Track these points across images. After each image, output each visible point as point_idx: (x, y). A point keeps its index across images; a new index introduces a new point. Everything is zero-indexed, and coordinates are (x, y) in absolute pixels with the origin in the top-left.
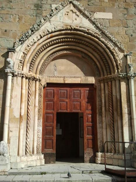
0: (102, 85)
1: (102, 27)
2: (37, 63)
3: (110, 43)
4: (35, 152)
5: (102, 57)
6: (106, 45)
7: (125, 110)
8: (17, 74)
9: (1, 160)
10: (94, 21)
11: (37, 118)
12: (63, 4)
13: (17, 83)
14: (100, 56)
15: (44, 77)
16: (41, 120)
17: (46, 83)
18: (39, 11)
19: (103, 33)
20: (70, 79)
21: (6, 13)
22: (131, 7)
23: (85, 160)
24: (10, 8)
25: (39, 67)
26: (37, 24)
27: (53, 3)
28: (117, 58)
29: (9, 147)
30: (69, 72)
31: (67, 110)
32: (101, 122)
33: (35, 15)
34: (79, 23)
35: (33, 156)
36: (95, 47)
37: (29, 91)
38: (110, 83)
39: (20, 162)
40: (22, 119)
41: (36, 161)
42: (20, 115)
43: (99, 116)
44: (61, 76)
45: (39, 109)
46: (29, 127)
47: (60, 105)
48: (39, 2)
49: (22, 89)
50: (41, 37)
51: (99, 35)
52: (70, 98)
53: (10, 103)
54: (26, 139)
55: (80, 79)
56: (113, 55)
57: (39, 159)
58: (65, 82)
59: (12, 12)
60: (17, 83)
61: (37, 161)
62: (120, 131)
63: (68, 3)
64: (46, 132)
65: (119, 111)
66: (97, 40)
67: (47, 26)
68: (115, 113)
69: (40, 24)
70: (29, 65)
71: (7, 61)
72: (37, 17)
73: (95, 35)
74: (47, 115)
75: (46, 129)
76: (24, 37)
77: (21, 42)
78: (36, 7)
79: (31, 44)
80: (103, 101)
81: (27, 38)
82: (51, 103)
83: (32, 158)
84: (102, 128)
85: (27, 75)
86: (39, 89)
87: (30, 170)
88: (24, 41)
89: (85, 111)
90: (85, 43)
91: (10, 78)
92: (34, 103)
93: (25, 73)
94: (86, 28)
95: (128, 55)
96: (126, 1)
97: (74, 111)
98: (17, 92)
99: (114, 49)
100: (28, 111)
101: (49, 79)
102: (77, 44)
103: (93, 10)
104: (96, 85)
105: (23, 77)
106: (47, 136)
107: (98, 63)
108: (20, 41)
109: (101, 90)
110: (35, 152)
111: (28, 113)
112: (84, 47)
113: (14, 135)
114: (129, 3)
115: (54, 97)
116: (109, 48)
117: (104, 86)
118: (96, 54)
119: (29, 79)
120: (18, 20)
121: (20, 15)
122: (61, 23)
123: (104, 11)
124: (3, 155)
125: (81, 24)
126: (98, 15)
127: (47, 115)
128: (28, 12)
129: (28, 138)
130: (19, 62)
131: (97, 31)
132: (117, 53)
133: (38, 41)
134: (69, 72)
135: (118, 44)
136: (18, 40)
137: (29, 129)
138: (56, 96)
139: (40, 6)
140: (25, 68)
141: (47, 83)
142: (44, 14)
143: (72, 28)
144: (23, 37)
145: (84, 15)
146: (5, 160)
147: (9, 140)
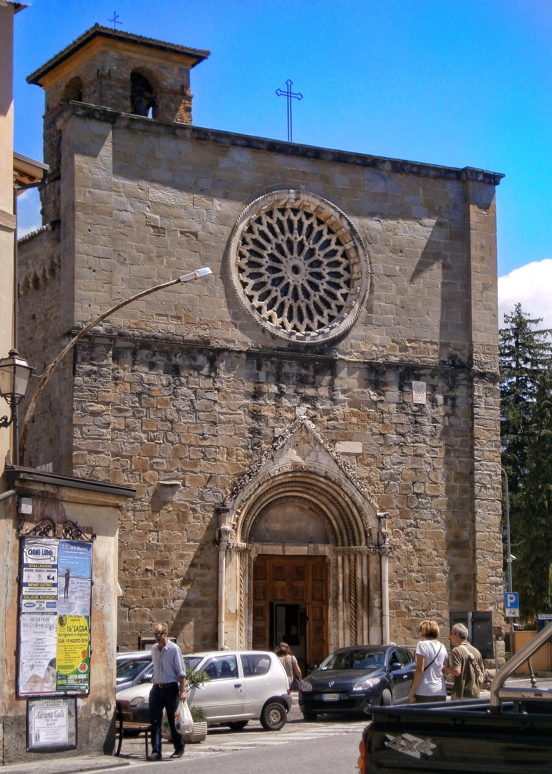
0: (340, 558)
5: (342, 511)
7: (490, 469)
14: (340, 512)
27: (277, 425)
32: (337, 618)
33: (250, 447)
36: (333, 497)
38: (352, 558)
43: (222, 649)
58: (284, 552)
62: (365, 632)
68: (360, 605)
80: (341, 585)
84: (337, 627)
102: (306, 490)
104: (330, 558)
107: (334, 522)
109: (337, 567)
112: (316, 494)
116: (354, 503)
118: (333, 508)
126: (342, 447)
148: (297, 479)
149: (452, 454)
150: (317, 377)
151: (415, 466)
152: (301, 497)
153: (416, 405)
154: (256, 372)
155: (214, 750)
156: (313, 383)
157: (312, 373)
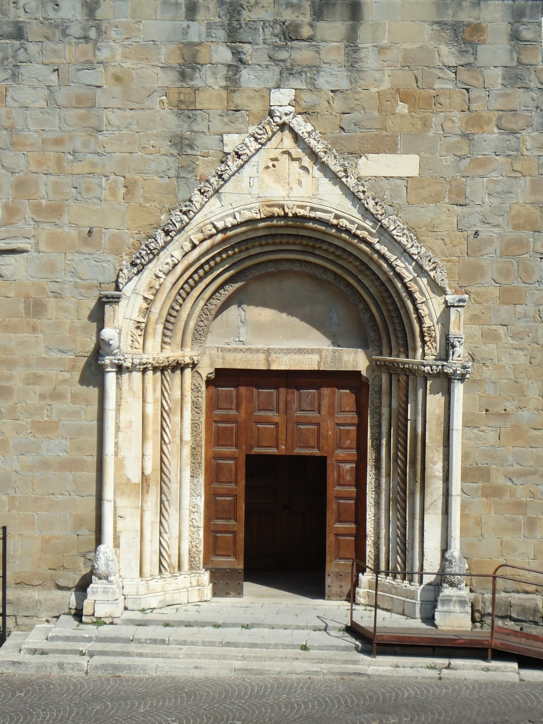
1: (380, 212)
2: (184, 315)
3: (402, 262)
4: (186, 566)
6: (393, 268)
8: (129, 365)
9: (103, 592)
10: (355, 191)
11: (187, 473)
12: (259, 137)
13: (131, 388)
15: (207, 353)
16: (202, 479)
17: (212, 370)
19: (383, 230)
20: (287, 358)
21: (88, 171)
22: (485, 128)
23: (326, 591)
24: (98, 154)
25: (192, 324)
26: (181, 211)
27: (228, 128)
28: (424, 310)
29: (118, 557)
30: (283, 339)
31: (277, 447)
33: (172, 173)
34: (311, 195)
35: (181, 578)
37: (163, 551)
39: (146, 594)
40: (148, 486)
41: (188, 591)
42: (143, 473)
44: (260, 346)
45: (194, 448)
46: (166, 503)
47: (256, 432)
48: (186, 126)
49: (144, 401)
50: (194, 246)
51: (371, 234)
52: (286, 413)
53: (116, 444)
54: (160, 533)
55: (316, 357)
56: (414, 301)
57: (196, 584)
59: (104, 166)
60: (131, 388)
61: (192, 588)
62: (417, 523)
63: (276, 128)
64: (214, 509)
65: (419, 467)
66: (367, 249)
67: (211, 212)
69: (188, 208)
70: (160, 327)
71: (103, 340)
72: (179, 180)
74: (219, 462)
75: (216, 502)
76: (144, 253)
77: (135, 270)
78: (175, 144)
79: (166, 268)
81: (151, 256)
82: (229, 427)
83: (177, 583)
85: (157, 363)
86: (193, 387)
87: (170, 614)
88: (143, 266)
89: (333, 452)
91: (111, 378)
92: (178, 433)
93: (151, 361)
94: (331, 212)
95: (454, 306)
96: (472, 109)
97: (299, 451)
99: (414, 280)
100: (160, 560)
103: (355, 147)
105: (144, 371)
106: (219, 522)
108: (133, 264)
109: (379, 392)
110: (186, 566)
111: (163, 466)
113: (129, 526)
114: (481, 116)
115: (238, 408)
116: (401, 278)
117: (388, 383)
119: (163, 370)
120: (125, 194)
121: (127, 175)
122: (254, 200)
123: (393, 150)
124: (108, 579)
125: (314, 201)
127: (219, 462)
128: (153, 166)
129: (166, 533)
130: (132, 325)
131: (368, 224)
132: (422, 294)
133: (184, 256)
134: (283, 339)
135: (427, 268)
136: (126, 263)
137: (168, 508)
138: (243, 406)
139: (187, 142)
140: (150, 343)
141: (217, 370)
142: (201, 171)
143: (286, 214)
144: (140, 253)
145: (324, 168)
146: (112, 590)
147: (116, 538)
150: (320, 25)
154: (185, 24)
155: (527, 592)
156: (310, 39)
157: (307, 18)
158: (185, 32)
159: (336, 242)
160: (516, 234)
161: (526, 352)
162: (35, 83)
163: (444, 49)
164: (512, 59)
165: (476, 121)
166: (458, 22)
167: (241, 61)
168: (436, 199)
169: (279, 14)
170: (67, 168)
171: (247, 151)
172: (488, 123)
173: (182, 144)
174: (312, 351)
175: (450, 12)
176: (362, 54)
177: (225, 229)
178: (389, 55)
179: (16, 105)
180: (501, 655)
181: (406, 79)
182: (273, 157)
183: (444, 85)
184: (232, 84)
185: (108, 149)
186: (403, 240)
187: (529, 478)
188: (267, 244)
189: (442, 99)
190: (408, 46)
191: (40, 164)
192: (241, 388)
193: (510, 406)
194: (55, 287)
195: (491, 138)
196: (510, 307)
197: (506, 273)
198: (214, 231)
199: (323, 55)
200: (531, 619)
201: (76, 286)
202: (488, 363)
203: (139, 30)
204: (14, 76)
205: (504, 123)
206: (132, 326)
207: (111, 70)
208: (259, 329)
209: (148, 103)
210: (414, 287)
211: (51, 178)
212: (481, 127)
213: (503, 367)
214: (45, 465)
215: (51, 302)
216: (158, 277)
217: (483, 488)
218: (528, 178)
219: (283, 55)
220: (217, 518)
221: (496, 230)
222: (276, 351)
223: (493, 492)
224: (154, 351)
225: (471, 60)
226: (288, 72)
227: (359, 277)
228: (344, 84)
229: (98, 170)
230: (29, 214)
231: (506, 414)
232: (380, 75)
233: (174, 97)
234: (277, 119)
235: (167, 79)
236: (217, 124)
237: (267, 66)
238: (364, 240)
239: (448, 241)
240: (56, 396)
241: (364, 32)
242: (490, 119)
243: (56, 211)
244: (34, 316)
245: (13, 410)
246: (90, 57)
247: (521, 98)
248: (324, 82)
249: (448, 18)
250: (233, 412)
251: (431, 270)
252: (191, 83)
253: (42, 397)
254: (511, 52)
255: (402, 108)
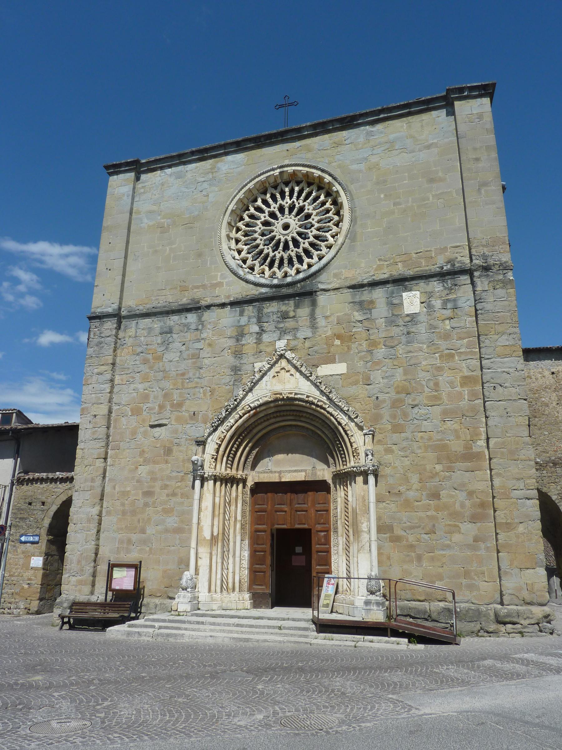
11: (238, 538)
16: (247, 542)
18: (237, 377)
22: (378, 346)
24: (199, 378)
27: (256, 360)
33: (231, 383)
35: (232, 595)
51: (325, 404)
55: (304, 474)
73: (318, 403)
90: (308, 416)
98: (207, 503)
101: (259, 477)
102: (297, 418)
103: (316, 363)
106: (257, 566)
113: (204, 563)
125: (296, 390)
126: (324, 370)
135: (353, 417)
142: (244, 381)
145: (301, 373)
148: (279, 409)
149: (457, 358)
151: (409, 377)
152: (295, 426)
153: (408, 315)
156: (294, 317)
158: (239, 322)
159: (309, 411)
160: (398, 396)
161: (408, 458)
162: (175, 350)
163: (356, 314)
164: (389, 314)
165: (373, 344)
166: (362, 301)
167: (262, 330)
168: (356, 383)
169: (280, 308)
170: (186, 386)
171: (264, 369)
172: (379, 344)
173: (236, 370)
174: (301, 471)
175: (358, 297)
176: (318, 320)
177: (255, 408)
178: (330, 319)
179: (167, 361)
180: (396, 633)
181: (339, 330)
182: (277, 371)
183: (359, 329)
184: (259, 341)
185: (204, 376)
186: (340, 404)
187: (416, 530)
188: (277, 416)
189: (356, 336)
190: (339, 314)
191: (174, 385)
192: (268, 494)
193: (402, 489)
194: (177, 441)
195: (381, 352)
196: (398, 435)
197: (394, 417)
198: (249, 408)
199: (300, 323)
200: (423, 617)
201: (186, 439)
202: (388, 465)
203: (220, 323)
204: (167, 348)
205: (387, 343)
206: (210, 457)
207: (207, 341)
208: (278, 463)
209: (222, 354)
210: (347, 428)
211: (179, 391)
212: (376, 346)
213: (397, 467)
214: (167, 531)
215: (175, 448)
216: (223, 433)
217: (390, 537)
218: (401, 368)
219: (281, 325)
220: (257, 564)
221: (387, 395)
222: (284, 472)
223: (396, 539)
224: (222, 470)
225: (369, 316)
226: (283, 332)
227: (323, 429)
228: (309, 334)
229: (199, 385)
230: (168, 408)
231: (400, 493)
232: (326, 328)
233: (233, 349)
234: (278, 353)
235: (231, 343)
236: (252, 359)
237: (274, 331)
238: (321, 407)
239: (363, 403)
240: (174, 494)
241: (318, 311)
242: (380, 342)
243: (180, 405)
244: (167, 456)
245: (154, 503)
246: (199, 337)
247: (395, 331)
248: (301, 335)
249: (357, 299)
250: (265, 506)
251: (355, 418)
252: (241, 343)
253: (168, 495)
254: (388, 310)
255: (337, 342)
